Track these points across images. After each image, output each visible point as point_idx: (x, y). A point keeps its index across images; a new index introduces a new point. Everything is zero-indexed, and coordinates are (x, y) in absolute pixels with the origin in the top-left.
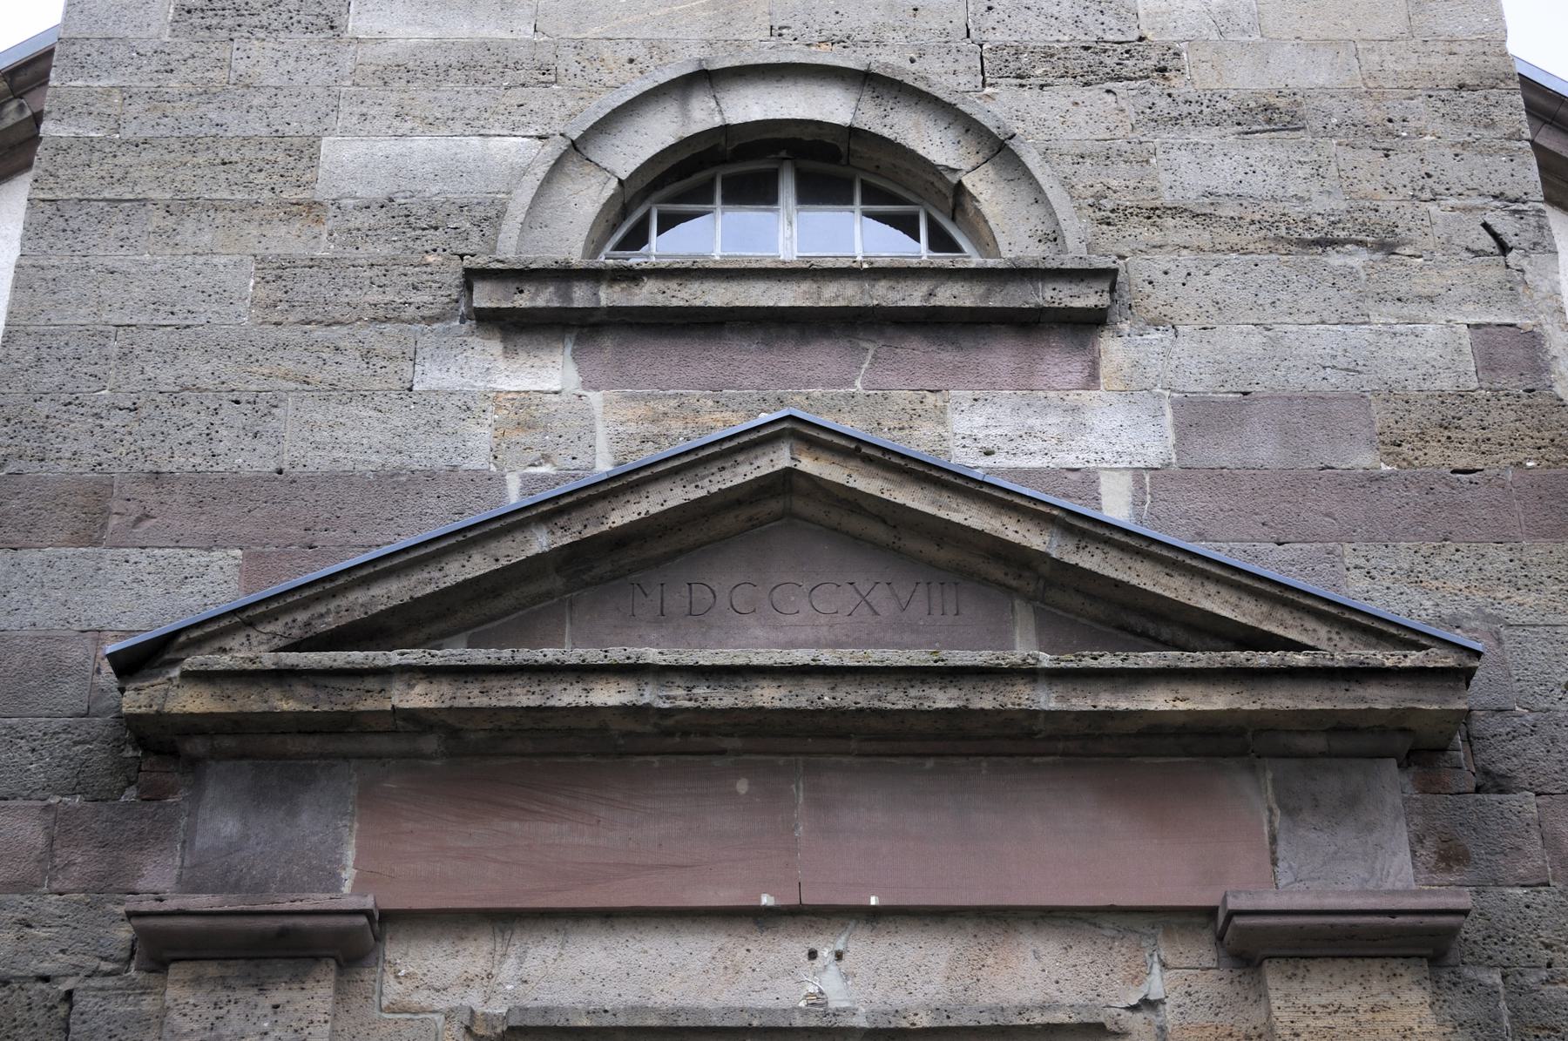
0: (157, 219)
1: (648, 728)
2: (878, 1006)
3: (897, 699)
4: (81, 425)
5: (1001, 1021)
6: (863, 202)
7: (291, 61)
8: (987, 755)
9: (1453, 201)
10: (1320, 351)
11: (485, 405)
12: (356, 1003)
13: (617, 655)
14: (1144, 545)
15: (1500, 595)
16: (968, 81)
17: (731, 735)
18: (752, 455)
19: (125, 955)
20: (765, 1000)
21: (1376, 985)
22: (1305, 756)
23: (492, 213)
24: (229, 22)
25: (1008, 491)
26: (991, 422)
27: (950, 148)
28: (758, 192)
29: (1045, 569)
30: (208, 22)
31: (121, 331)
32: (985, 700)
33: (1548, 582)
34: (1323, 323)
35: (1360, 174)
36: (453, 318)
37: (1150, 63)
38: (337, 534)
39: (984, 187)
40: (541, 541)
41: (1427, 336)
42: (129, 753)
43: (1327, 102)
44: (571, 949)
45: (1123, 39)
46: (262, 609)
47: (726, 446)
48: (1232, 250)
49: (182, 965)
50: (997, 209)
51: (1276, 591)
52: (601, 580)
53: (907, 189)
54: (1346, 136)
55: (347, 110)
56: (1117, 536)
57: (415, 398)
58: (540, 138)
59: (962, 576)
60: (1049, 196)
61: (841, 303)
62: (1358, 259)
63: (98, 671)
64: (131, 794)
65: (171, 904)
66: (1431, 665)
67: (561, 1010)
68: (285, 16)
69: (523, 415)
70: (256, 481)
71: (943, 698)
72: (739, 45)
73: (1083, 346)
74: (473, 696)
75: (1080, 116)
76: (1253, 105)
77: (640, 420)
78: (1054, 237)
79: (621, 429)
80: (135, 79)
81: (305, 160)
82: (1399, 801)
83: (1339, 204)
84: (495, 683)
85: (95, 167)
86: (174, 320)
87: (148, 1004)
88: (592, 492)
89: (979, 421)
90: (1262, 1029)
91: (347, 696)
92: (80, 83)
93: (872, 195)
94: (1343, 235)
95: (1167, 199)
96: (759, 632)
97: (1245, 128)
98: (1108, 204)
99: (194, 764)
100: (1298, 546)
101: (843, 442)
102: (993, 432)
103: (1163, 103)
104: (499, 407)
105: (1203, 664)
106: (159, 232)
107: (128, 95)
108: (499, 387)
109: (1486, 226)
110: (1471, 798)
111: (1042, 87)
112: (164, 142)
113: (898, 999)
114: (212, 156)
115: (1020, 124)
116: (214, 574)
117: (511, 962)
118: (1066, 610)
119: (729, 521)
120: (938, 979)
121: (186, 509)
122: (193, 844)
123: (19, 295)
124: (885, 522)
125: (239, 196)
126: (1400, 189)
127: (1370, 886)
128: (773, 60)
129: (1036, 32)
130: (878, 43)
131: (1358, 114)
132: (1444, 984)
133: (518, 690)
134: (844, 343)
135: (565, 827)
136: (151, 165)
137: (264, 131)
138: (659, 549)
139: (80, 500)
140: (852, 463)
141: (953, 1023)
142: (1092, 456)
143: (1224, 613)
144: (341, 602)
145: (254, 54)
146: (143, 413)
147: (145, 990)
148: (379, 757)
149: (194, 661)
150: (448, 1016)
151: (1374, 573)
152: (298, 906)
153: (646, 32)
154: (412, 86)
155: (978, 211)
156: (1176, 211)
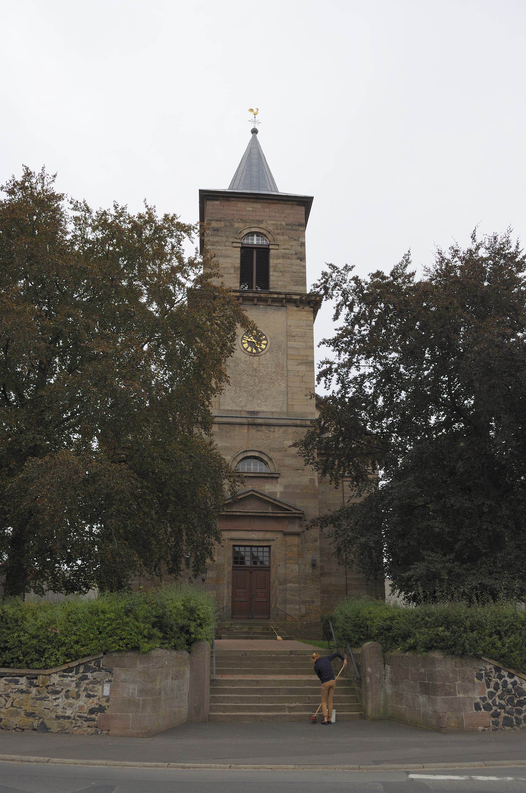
62: (300, 471)
83: (300, 466)
156: (285, 466)
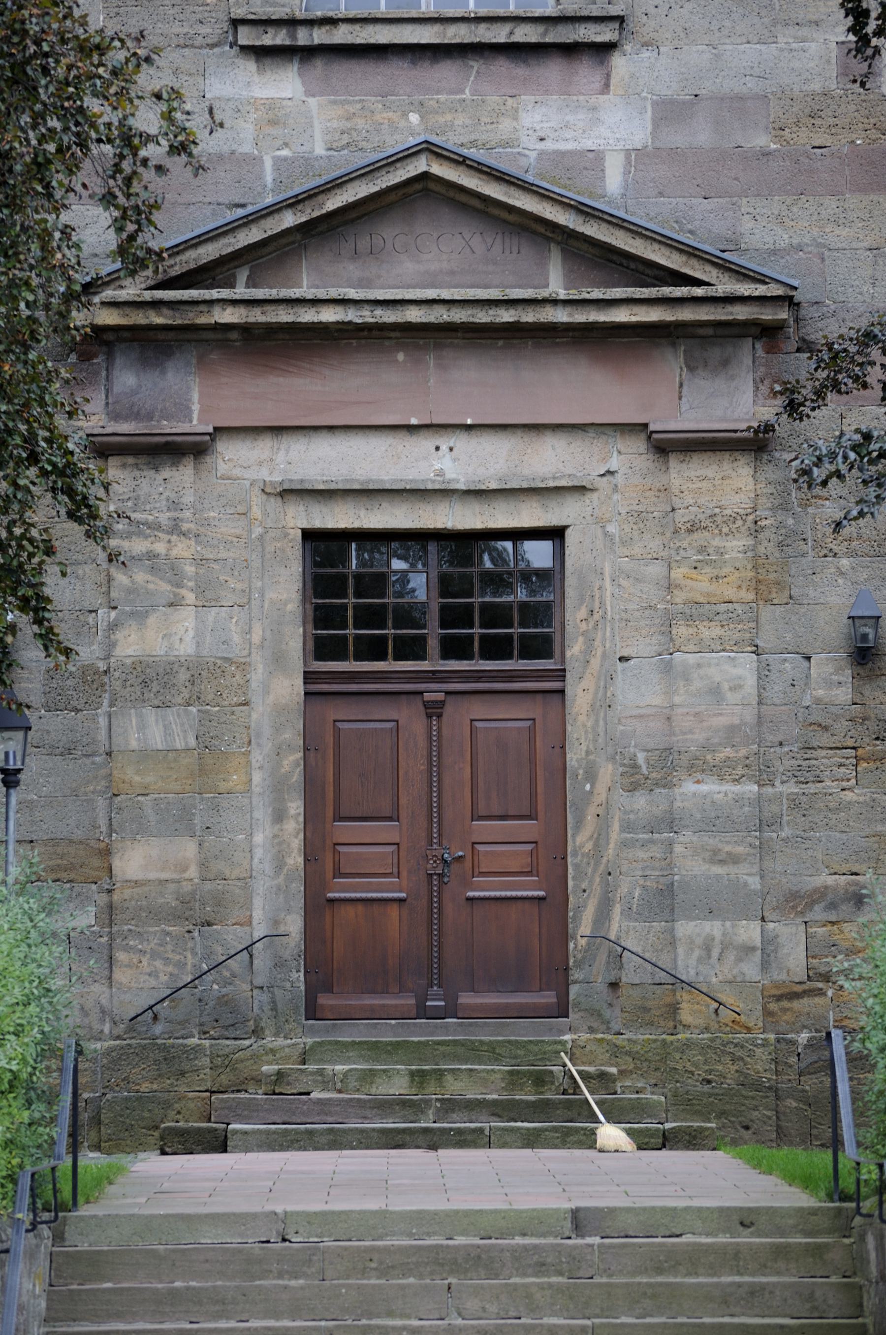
5: (533, 486)
10: (745, 64)
11: (248, 108)
13: (333, 293)
14: (620, 222)
15: (827, 230)
25: (547, 190)
26: (544, 118)
34: (748, 42)
36: (226, 43)
40: (289, 220)
51: (691, 250)
52: (321, 233)
67: (310, 481)
73: (602, 63)
74: (257, 316)
79: (329, 125)
84: (269, 308)
89: (538, 117)
91: (191, 315)
100: (716, 200)
102: (545, 125)
104: (256, 109)
108: (256, 95)
110: (793, 356)
117: (282, 453)
132: (764, 461)
133: (281, 312)
134: (459, 62)
141: (508, 487)
151: (757, 217)
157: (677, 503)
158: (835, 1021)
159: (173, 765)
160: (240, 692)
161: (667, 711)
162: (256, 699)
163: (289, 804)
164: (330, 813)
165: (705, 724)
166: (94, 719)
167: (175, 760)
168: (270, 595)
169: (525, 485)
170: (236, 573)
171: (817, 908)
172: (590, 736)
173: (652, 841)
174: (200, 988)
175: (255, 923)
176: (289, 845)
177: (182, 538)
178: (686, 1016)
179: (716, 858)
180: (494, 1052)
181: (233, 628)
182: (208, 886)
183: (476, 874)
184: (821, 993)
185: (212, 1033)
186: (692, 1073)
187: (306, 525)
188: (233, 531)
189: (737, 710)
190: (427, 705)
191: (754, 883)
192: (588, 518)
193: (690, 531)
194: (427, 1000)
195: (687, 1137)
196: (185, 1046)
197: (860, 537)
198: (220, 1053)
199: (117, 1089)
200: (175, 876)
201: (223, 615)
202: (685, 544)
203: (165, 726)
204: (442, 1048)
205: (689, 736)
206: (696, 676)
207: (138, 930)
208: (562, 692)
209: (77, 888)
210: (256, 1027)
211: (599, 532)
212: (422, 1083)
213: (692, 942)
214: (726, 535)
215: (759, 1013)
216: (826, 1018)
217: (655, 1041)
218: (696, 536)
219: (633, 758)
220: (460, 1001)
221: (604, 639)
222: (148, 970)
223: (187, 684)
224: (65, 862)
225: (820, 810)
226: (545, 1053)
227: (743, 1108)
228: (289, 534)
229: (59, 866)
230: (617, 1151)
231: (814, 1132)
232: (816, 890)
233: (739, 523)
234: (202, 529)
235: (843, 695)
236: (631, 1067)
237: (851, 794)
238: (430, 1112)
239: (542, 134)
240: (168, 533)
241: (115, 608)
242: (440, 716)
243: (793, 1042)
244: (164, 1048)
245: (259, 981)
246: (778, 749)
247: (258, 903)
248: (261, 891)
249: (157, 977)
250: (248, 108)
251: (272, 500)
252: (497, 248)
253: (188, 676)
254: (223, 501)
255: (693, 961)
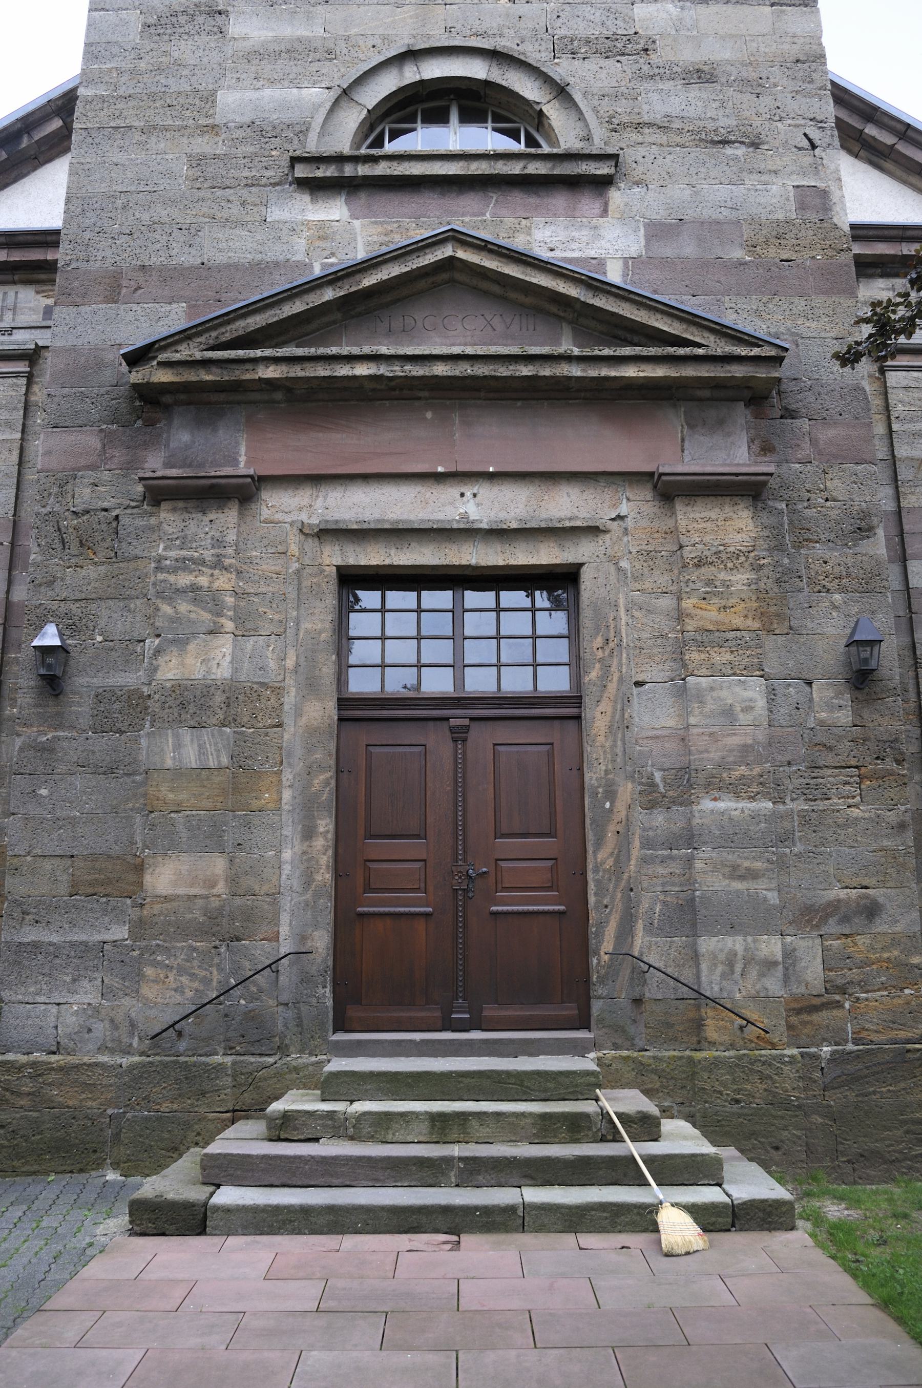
0: (137, 136)
1: (383, 387)
2: (493, 518)
3: (503, 371)
4: (105, 243)
5: (550, 525)
6: (493, 122)
7: (201, 51)
8: (546, 399)
9: (789, 122)
11: (302, 228)
12: (249, 518)
13: (366, 350)
15: (799, 323)
16: (546, 56)
17: (423, 390)
18: (433, 249)
19: (141, 498)
20: (440, 516)
21: (727, 509)
22: (700, 400)
23: (304, 128)
24: (169, 31)
27: (536, 91)
28: (438, 117)
29: (578, 306)
30: (159, 31)
31: (122, 195)
32: (546, 371)
33: (823, 316)
35: (744, 106)
36: (285, 183)
37: (640, 47)
38: (232, 294)
39: (554, 113)
40: (329, 294)
41: (772, 191)
42: (137, 403)
43: (729, 68)
44: (348, 493)
45: (626, 33)
46: (194, 330)
47: (420, 244)
48: (677, 145)
49: (167, 502)
50: (559, 124)
51: (690, 317)
52: (359, 315)
53: (515, 115)
54: (738, 86)
55: (230, 76)
56: (613, 290)
57: (268, 225)
58: (328, 88)
59: (537, 311)
60: (586, 116)
61: (480, 172)
63: (121, 364)
64: (139, 423)
65: (159, 474)
66: (763, 355)
67: (344, 521)
68: (197, 27)
69: (321, 233)
70: (192, 269)
71: (526, 371)
72: (429, 37)
73: (601, 195)
74: (297, 371)
75: (603, 75)
76: (691, 69)
77: (379, 234)
78: (588, 138)
80: (123, 63)
81: (210, 103)
82: (743, 422)
83: (733, 122)
84: (308, 365)
85: (106, 110)
86: (148, 188)
87: (153, 521)
88: (354, 269)
89: (548, 233)
90: (672, 529)
91: (237, 372)
92: (96, 66)
93: (497, 118)
94: (733, 138)
95: (646, 119)
96: (437, 340)
97: (687, 81)
98: (616, 121)
99: (167, 408)
101: (479, 242)
102: (555, 239)
103: (646, 68)
104: (309, 229)
105: (653, 354)
106: (139, 143)
107: (120, 73)
108: (309, 219)
109: (805, 135)
110: (778, 421)
111: (584, 59)
112: (139, 96)
113: (502, 515)
114: (163, 102)
115: (572, 79)
116: (173, 316)
117: (320, 499)
118: (587, 328)
119: (422, 284)
120: (521, 506)
121: (158, 283)
122: (169, 445)
123: (72, 178)
124: (499, 284)
125: (177, 123)
126: (764, 115)
127: (728, 462)
128: (446, 44)
129: (582, 29)
130: (501, 36)
131: (744, 74)
132: (759, 508)
134: (481, 194)
135: (344, 436)
136: (133, 108)
137: (189, 88)
138: (388, 298)
139: (108, 281)
140: (483, 253)
141: (528, 526)
142: (604, 251)
143: (664, 329)
144: (233, 327)
145: (182, 48)
146: (135, 236)
147: (151, 514)
148: (255, 402)
149: (163, 357)
150: (292, 524)
151: (739, 311)
152: (218, 473)
153: (381, 31)
154: (262, 63)
155: (550, 125)
156: (650, 125)
157: (684, 540)
158: (853, 1033)
159: (205, 783)
160: (274, 714)
161: (682, 732)
162: (288, 720)
163: (319, 822)
164: (361, 832)
165: (720, 743)
166: (136, 740)
167: (208, 779)
168: (306, 625)
169: (543, 525)
170: (275, 606)
171: (831, 921)
172: (609, 756)
173: (671, 858)
174: (228, 1003)
175: (281, 939)
176: (317, 861)
177: (224, 572)
178: (711, 1032)
179: (736, 873)
180: (522, 1086)
181: (270, 655)
182: (238, 901)
183: (499, 888)
184: (839, 1005)
185: (238, 1048)
186: (720, 1093)
187: (340, 563)
188: (273, 568)
189: (750, 730)
190: (452, 730)
191: (773, 898)
192: (601, 556)
193: (698, 566)
194: (452, 1012)
195: (761, 1215)
196: (207, 1064)
197: (848, 575)
198: (244, 1071)
199: (138, 1108)
200: (203, 892)
201: (261, 643)
202: (694, 578)
203: (199, 745)
204: (467, 1081)
205: (706, 755)
206: (709, 698)
207: (166, 945)
208: (578, 718)
209: (113, 902)
210: (282, 1044)
211: (612, 569)
212: (443, 1129)
213: (715, 958)
214: (731, 569)
215: (783, 1029)
216: (845, 1031)
217: (681, 1058)
218: (703, 570)
219: (651, 777)
220: (485, 1013)
221: (620, 665)
222: (174, 986)
223: (222, 705)
224: (103, 877)
225: (830, 826)
226: (576, 1086)
227: (773, 1128)
228: (325, 571)
229: (96, 880)
230: (688, 1253)
231: (841, 1148)
232: (829, 904)
233: (742, 559)
234: (245, 567)
235: (844, 717)
236: (658, 1085)
237: (857, 811)
238: (453, 1173)
239: (552, 246)
240: (211, 568)
241: (158, 636)
242: (465, 740)
243: (816, 1057)
244: (186, 1066)
245: (284, 997)
246: (786, 768)
247: (285, 918)
248: (287, 907)
249: (183, 993)
250: (302, 228)
251: (310, 540)
252: (515, 327)
253: (224, 698)
254: (265, 542)
255: (716, 977)
